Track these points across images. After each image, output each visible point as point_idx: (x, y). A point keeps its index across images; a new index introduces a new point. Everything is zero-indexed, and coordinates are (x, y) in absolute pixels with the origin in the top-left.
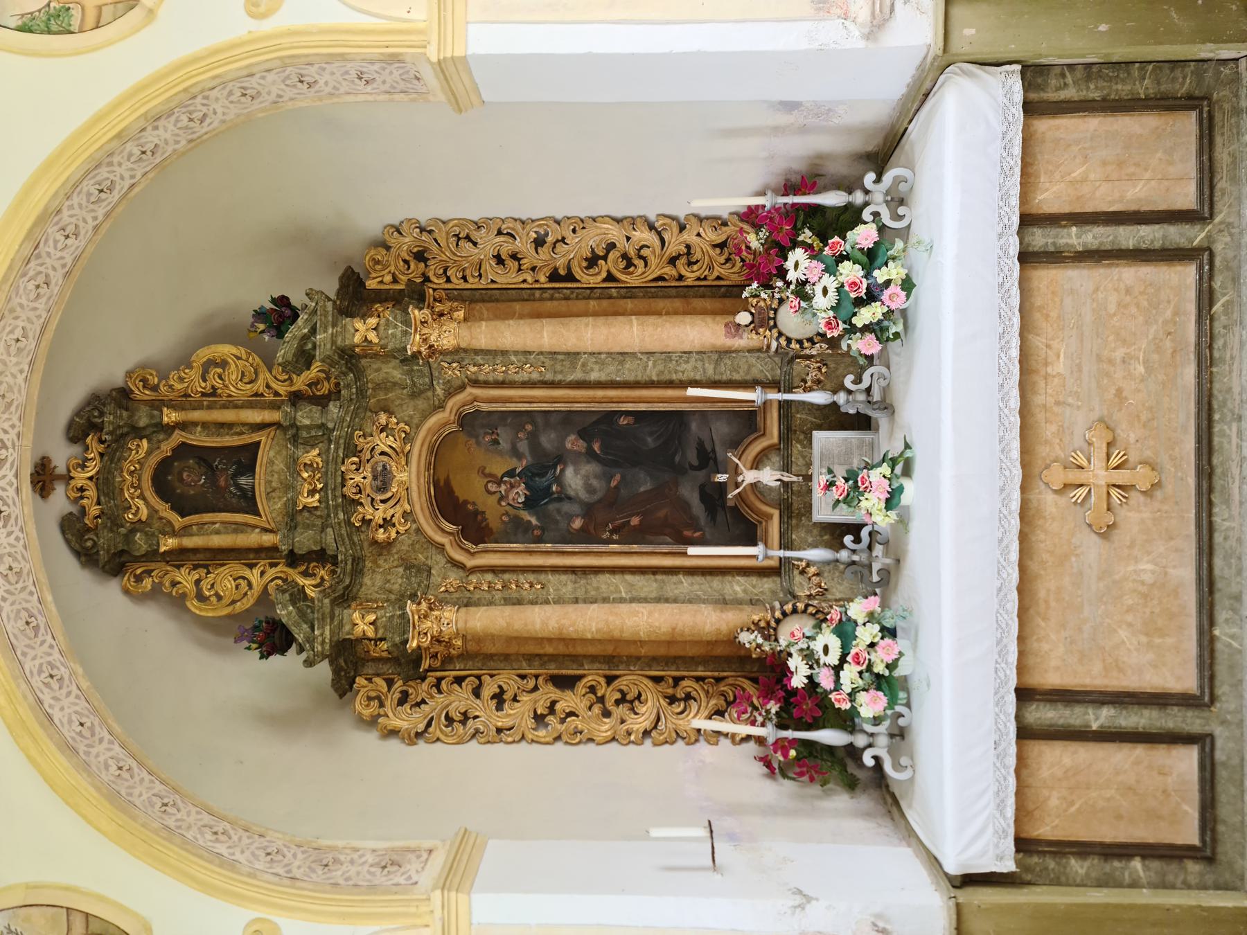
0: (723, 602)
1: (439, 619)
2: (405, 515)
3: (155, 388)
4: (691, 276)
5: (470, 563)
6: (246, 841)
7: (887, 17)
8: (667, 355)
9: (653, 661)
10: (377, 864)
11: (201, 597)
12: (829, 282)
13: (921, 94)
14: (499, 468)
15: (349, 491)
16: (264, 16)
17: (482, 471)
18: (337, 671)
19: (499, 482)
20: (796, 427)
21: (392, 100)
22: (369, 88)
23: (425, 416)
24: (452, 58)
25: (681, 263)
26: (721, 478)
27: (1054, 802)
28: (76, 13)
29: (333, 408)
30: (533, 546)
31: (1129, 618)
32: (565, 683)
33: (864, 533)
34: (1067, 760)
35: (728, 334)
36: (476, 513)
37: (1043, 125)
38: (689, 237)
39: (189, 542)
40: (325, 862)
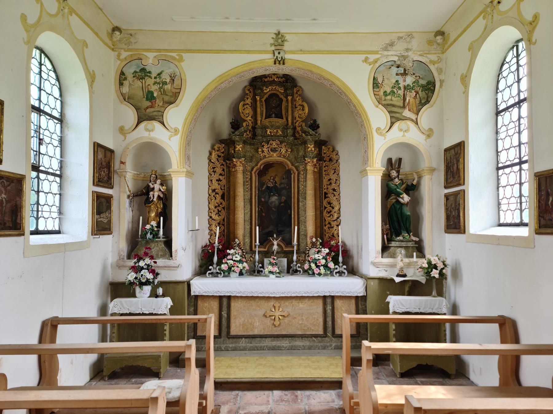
0: (244, 236)
1: (240, 166)
2: (265, 156)
3: (297, 93)
4: (326, 228)
5: (253, 173)
8: (305, 222)
9: (229, 219)
11: (244, 105)
12: (321, 257)
13: (362, 276)
14: (276, 180)
15: (271, 142)
17: (276, 175)
18: (226, 140)
19: (273, 180)
20: (288, 255)
23: (290, 161)
25: (329, 225)
26: (275, 236)
27: (206, 304)
28: (378, 90)
29: (292, 138)
30: (257, 188)
31: (246, 321)
32: (223, 197)
33: (262, 269)
34: (215, 307)
35: (310, 237)
36: (266, 174)
37: (353, 301)
38: (335, 227)
39: (258, 103)
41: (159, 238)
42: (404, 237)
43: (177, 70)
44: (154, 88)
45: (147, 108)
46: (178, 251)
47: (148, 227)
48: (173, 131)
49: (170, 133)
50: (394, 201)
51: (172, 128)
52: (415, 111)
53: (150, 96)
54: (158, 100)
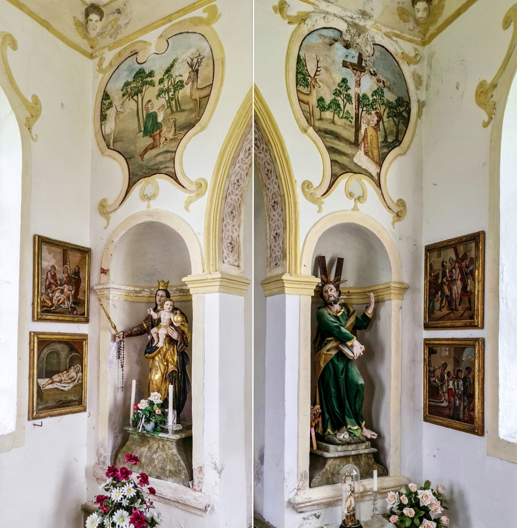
6: (244, 167)
7: (298, 510)
10: (232, 240)
16: (303, 190)
21: (267, 248)
22: (272, 237)
24: (284, 287)
40: (234, 212)
41: (166, 431)
42: (350, 434)
43: (205, 44)
44: (158, 106)
45: (146, 151)
46: (205, 470)
47: (143, 404)
48: (193, 188)
49: (188, 195)
50: (333, 353)
51: (191, 182)
52: (377, 159)
53: (151, 126)
54: (164, 129)
